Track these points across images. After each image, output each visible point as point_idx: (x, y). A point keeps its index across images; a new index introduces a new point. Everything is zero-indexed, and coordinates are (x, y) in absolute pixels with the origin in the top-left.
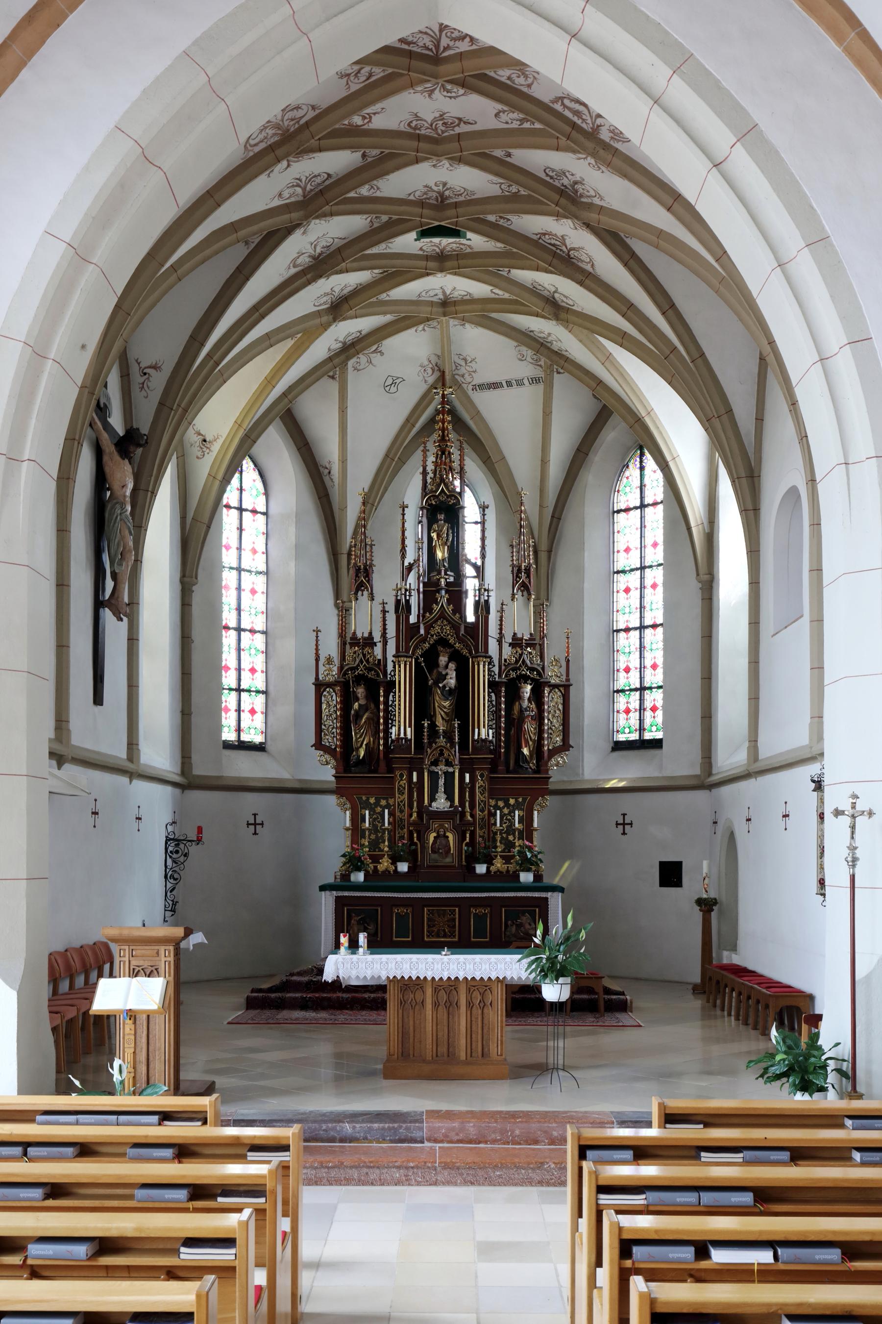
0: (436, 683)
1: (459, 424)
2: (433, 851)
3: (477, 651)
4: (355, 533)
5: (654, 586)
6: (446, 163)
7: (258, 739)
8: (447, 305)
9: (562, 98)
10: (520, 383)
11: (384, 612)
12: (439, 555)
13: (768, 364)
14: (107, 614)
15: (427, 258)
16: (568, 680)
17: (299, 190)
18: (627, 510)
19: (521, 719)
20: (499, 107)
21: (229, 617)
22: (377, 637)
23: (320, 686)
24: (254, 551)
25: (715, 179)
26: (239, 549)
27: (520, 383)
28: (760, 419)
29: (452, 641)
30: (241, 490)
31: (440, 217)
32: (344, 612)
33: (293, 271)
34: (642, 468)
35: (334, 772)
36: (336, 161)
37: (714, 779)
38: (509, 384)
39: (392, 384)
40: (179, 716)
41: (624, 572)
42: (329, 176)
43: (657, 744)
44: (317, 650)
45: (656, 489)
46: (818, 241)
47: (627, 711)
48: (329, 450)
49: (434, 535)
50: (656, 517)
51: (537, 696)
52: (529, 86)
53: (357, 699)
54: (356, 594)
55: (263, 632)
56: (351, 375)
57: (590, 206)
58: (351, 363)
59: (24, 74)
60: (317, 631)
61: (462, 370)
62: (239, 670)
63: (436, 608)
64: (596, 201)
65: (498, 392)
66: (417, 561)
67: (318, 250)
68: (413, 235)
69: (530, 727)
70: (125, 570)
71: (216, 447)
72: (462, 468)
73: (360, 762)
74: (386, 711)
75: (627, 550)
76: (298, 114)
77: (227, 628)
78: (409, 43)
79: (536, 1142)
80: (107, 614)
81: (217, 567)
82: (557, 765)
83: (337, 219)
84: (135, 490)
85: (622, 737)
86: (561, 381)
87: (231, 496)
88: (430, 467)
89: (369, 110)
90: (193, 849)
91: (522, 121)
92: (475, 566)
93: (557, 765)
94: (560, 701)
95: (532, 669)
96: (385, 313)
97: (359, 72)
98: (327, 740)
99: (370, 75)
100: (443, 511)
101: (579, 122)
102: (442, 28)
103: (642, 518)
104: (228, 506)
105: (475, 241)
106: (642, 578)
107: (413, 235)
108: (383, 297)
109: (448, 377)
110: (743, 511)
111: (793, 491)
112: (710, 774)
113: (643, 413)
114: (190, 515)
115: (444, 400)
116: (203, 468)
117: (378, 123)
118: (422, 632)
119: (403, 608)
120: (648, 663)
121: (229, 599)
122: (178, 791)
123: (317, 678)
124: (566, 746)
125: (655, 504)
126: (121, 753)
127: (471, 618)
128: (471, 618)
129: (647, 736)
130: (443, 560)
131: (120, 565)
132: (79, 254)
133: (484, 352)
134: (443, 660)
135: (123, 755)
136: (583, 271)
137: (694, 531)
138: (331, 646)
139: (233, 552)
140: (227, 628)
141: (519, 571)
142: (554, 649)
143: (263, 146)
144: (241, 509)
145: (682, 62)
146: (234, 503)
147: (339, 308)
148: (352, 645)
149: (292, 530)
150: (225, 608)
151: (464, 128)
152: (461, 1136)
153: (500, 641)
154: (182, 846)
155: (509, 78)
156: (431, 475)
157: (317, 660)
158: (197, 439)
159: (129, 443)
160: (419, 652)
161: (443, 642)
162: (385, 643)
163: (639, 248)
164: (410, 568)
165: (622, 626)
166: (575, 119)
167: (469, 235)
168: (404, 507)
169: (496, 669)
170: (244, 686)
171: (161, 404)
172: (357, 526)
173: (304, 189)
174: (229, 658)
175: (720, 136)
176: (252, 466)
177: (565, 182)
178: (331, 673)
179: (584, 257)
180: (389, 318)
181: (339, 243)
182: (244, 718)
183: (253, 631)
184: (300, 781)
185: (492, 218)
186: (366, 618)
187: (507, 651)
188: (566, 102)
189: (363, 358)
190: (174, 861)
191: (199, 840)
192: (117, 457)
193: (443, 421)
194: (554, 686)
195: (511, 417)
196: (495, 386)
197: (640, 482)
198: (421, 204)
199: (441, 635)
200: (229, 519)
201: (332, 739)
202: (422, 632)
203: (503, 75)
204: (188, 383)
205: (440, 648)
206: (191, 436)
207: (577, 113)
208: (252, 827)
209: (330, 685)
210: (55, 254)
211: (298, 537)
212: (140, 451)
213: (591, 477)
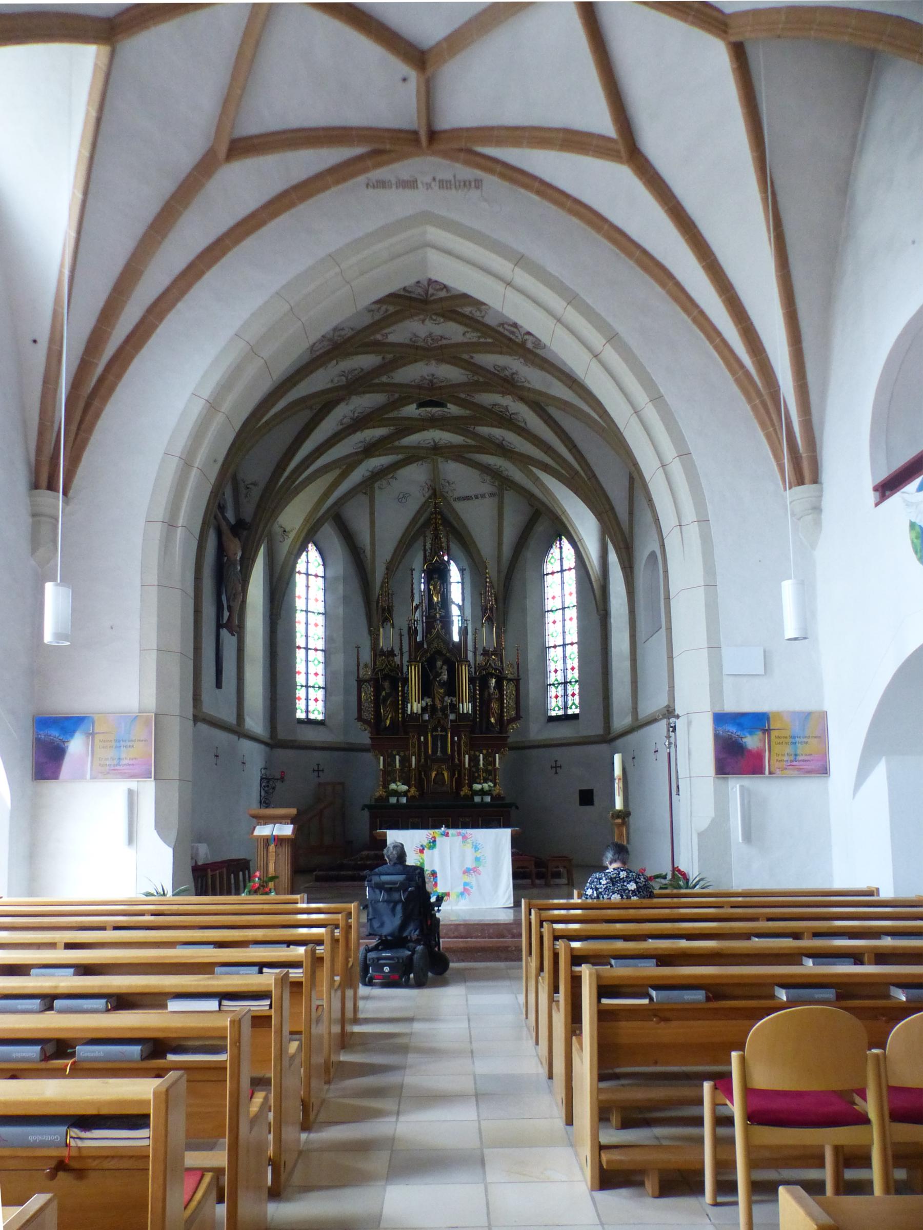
0: (435, 678)
1: (447, 523)
2: (435, 783)
3: (460, 657)
4: (382, 587)
5: (571, 619)
6: (433, 362)
7: (320, 717)
8: (437, 450)
9: (503, 324)
10: (483, 496)
11: (401, 635)
12: (435, 599)
13: (635, 481)
14: (224, 632)
15: (423, 420)
16: (518, 676)
17: (344, 379)
18: (553, 573)
19: (490, 701)
20: (466, 329)
21: (300, 641)
22: (397, 652)
23: (360, 682)
24: (317, 600)
25: (594, 364)
26: (307, 599)
27: (483, 496)
28: (631, 513)
29: (444, 652)
30: (308, 562)
31: (431, 395)
32: (374, 635)
33: (340, 427)
34: (561, 548)
35: (369, 735)
36: (366, 361)
37: (612, 735)
38: (476, 497)
39: (403, 498)
40: (268, 702)
41: (552, 611)
42: (362, 370)
43: (575, 717)
44: (358, 659)
45: (570, 558)
46: (657, 399)
47: (557, 697)
48: (364, 539)
49: (431, 587)
50: (571, 577)
51: (499, 685)
52: (483, 317)
53: (384, 689)
54: (383, 624)
55: (322, 650)
56: (377, 492)
57: (523, 388)
58: (376, 485)
59: (180, 305)
60: (358, 648)
61: (447, 489)
62: (307, 674)
63: (434, 632)
64: (526, 384)
65: (470, 502)
66: (421, 603)
67: (356, 415)
68: (414, 406)
69: (495, 705)
70: (236, 607)
71: (292, 535)
72: (448, 547)
73: (386, 729)
74: (403, 696)
75: (554, 598)
76: (343, 333)
77: (299, 648)
78: (410, 292)
79: (503, 937)
80: (224, 632)
81: (292, 610)
82: (513, 728)
83: (368, 395)
84: (241, 558)
85: (553, 714)
86: (510, 497)
87: (301, 566)
88: (428, 546)
89: (386, 331)
90: (278, 785)
91: (479, 337)
92: (458, 605)
93: (513, 728)
94: (514, 689)
95: (496, 669)
96: (398, 454)
97: (380, 308)
98: (366, 715)
99: (387, 310)
100: (437, 574)
101: (514, 338)
102: (430, 282)
103: (562, 577)
104: (299, 573)
105: (453, 409)
106: (563, 614)
107: (414, 406)
108: (396, 443)
109: (438, 493)
110: (624, 568)
111: (653, 555)
112: (609, 733)
113: (560, 513)
114: (276, 575)
115: (436, 506)
116: (284, 547)
117: (392, 338)
118: (425, 646)
119: (413, 632)
120: (569, 666)
121: (300, 629)
122: (268, 749)
123: (358, 677)
124: (518, 717)
125: (570, 569)
126: (232, 719)
127: (456, 638)
128: (456, 638)
129: (570, 712)
130: (438, 602)
131: (234, 601)
132: (213, 406)
133: (460, 477)
134: (439, 663)
135: (234, 722)
136: (520, 427)
137: (594, 583)
138: (366, 656)
139: (303, 601)
140: (299, 648)
141: (486, 609)
142: (509, 657)
143: (321, 351)
144: (307, 574)
145: (573, 299)
146: (303, 571)
147: (369, 450)
148: (380, 656)
149: (341, 588)
150: (298, 635)
151: (444, 342)
152: (456, 934)
153: (475, 653)
154: (271, 783)
155: (471, 312)
156: (429, 551)
157: (358, 666)
158: (280, 530)
159: (239, 527)
160: (424, 659)
161: (439, 652)
162: (402, 654)
163: (552, 411)
164: (417, 607)
165: (551, 644)
166: (511, 336)
167: (449, 405)
168: (412, 570)
169: (473, 670)
170: (310, 684)
171: (259, 506)
172: (383, 583)
173: (347, 378)
174: (300, 666)
175: (597, 340)
176: (315, 548)
177: (507, 373)
178: (367, 673)
179: (520, 419)
180: (400, 457)
181: (368, 410)
182: (310, 703)
183: (316, 650)
184: (347, 743)
185: (463, 396)
186: (388, 638)
187: (480, 659)
188: (506, 326)
189: (384, 482)
190: (266, 792)
191: (282, 779)
192: (230, 535)
193: (436, 519)
194: (509, 680)
195: (478, 517)
196: (467, 498)
197: (561, 556)
198: (419, 387)
199: (436, 655)
200: (300, 580)
201: (369, 715)
202: (425, 646)
203: (467, 310)
204: (275, 495)
205: (437, 657)
206: (276, 528)
207: (513, 333)
208: (316, 773)
209: (366, 681)
210: (198, 407)
211: (344, 591)
212: (245, 533)
213: (528, 555)
